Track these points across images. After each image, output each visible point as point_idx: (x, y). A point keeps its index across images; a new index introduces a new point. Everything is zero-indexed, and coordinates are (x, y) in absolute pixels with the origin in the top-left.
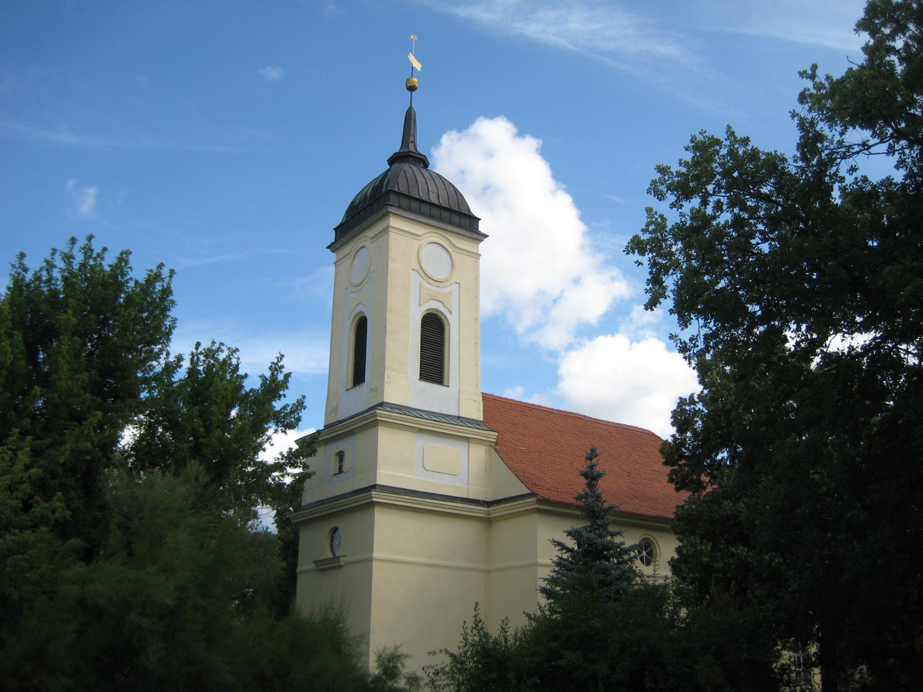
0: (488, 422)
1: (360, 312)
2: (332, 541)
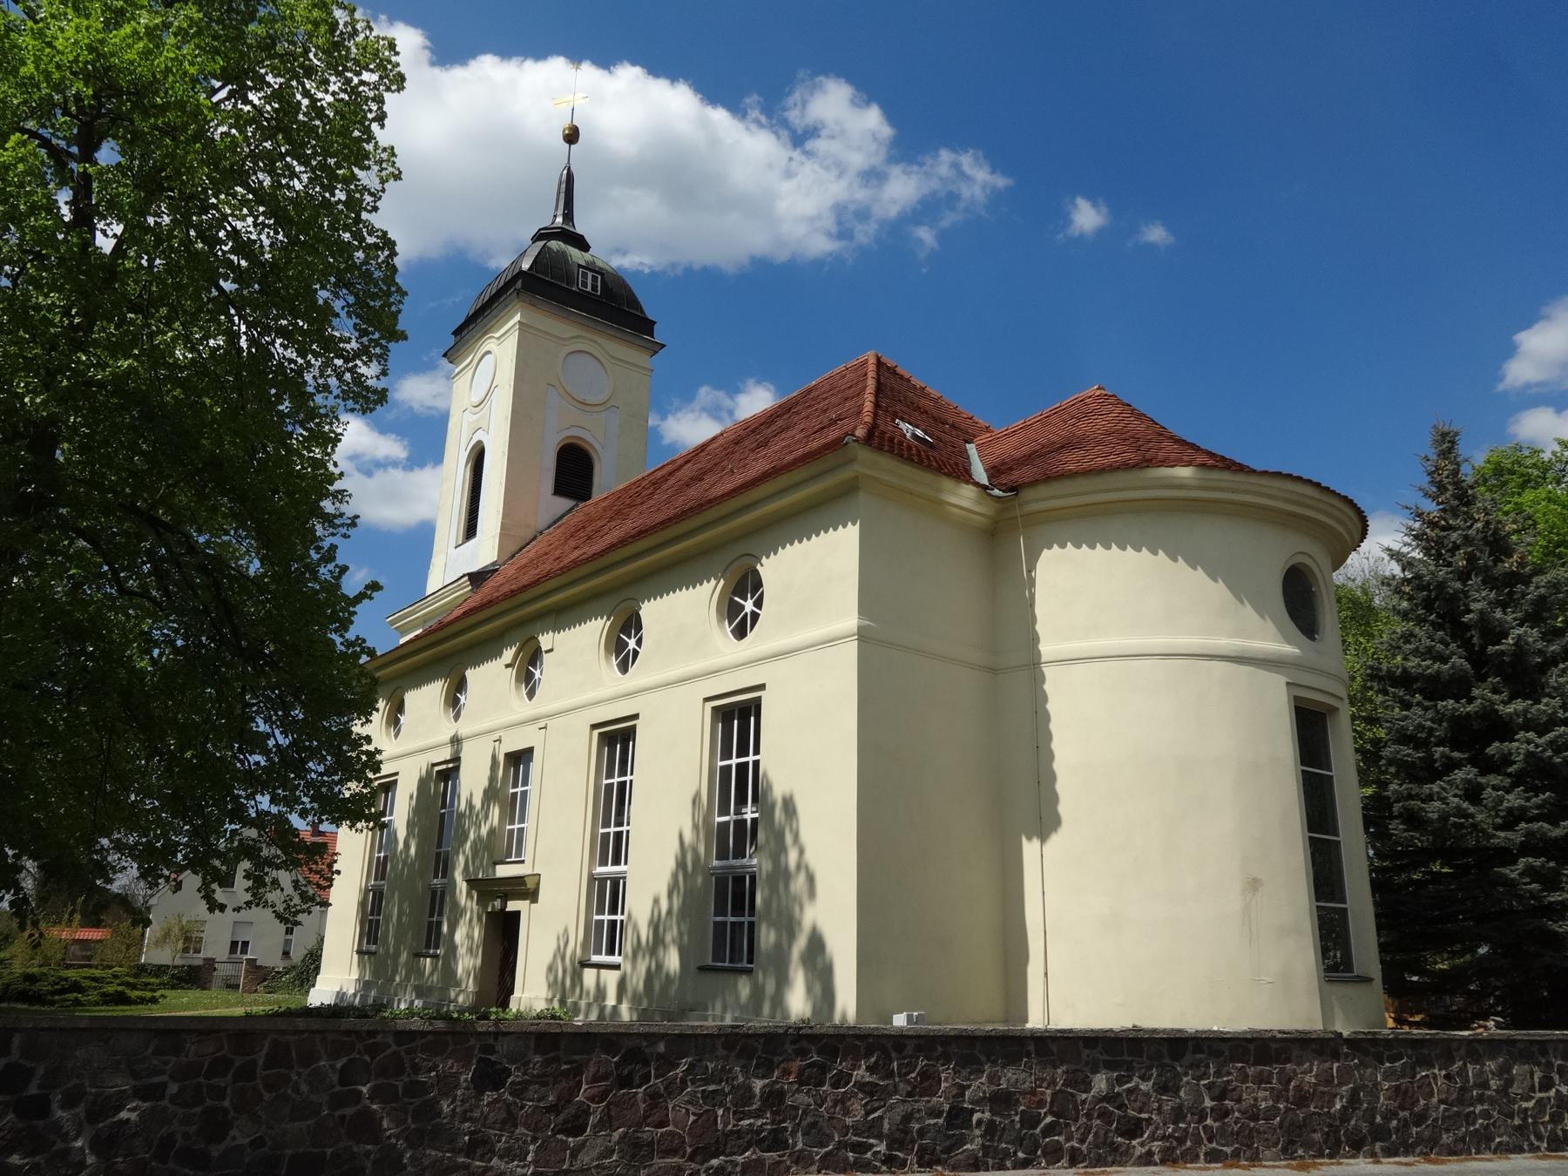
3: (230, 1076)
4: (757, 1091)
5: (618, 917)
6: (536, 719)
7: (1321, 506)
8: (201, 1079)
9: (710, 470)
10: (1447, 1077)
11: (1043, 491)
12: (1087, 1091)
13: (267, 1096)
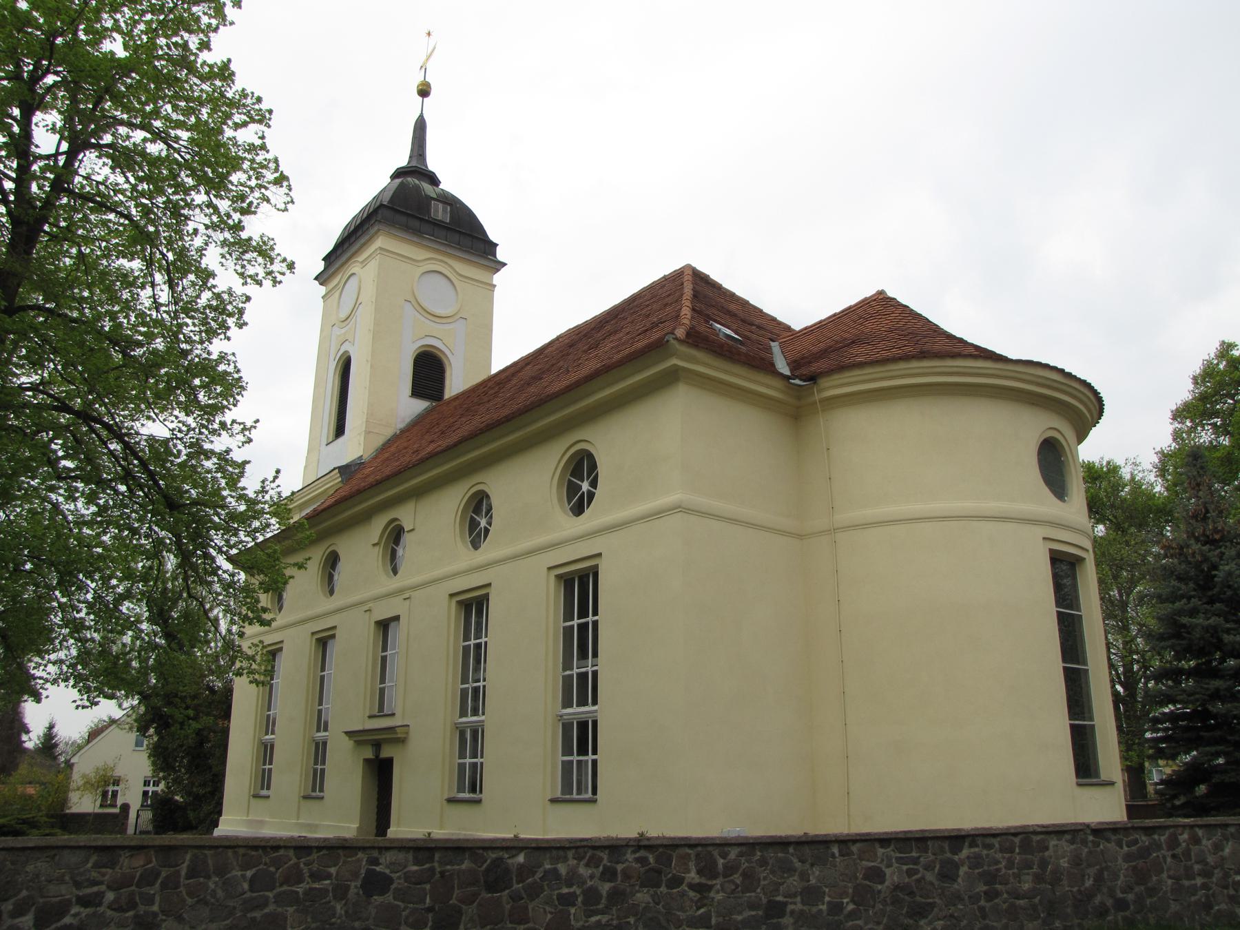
1: (346, 352)
3: (157, 885)
4: (604, 894)
5: (478, 760)
6: (400, 591)
7: (1064, 388)
8: (133, 888)
9: (548, 370)
10: (1174, 856)
11: (837, 379)
12: (882, 882)
13: (189, 901)
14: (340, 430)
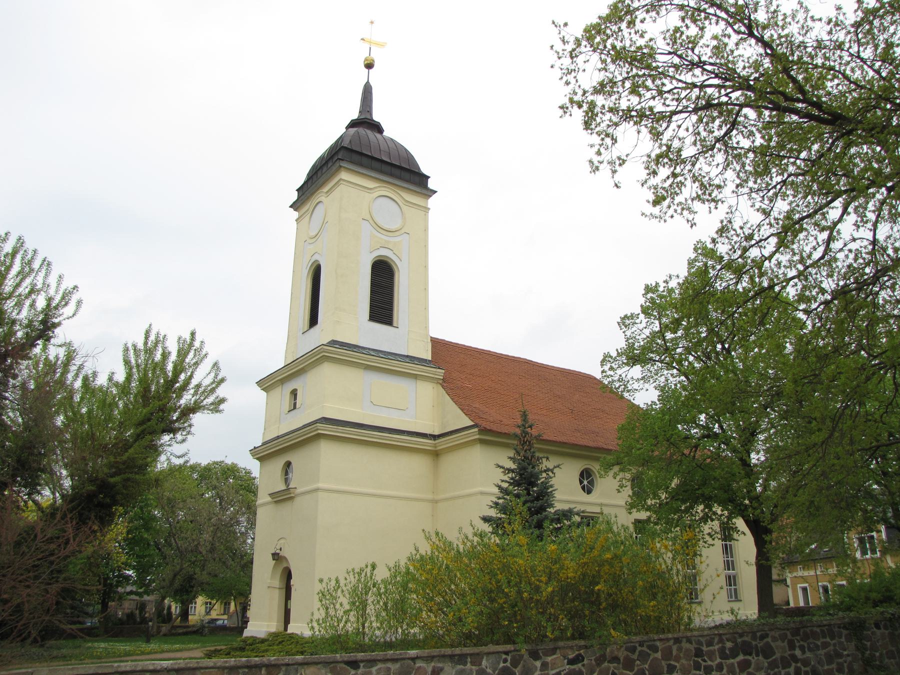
0: (435, 362)
1: (316, 261)
2: (287, 473)
14: (313, 320)
